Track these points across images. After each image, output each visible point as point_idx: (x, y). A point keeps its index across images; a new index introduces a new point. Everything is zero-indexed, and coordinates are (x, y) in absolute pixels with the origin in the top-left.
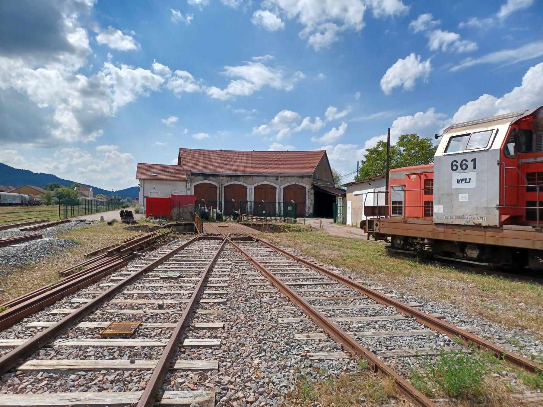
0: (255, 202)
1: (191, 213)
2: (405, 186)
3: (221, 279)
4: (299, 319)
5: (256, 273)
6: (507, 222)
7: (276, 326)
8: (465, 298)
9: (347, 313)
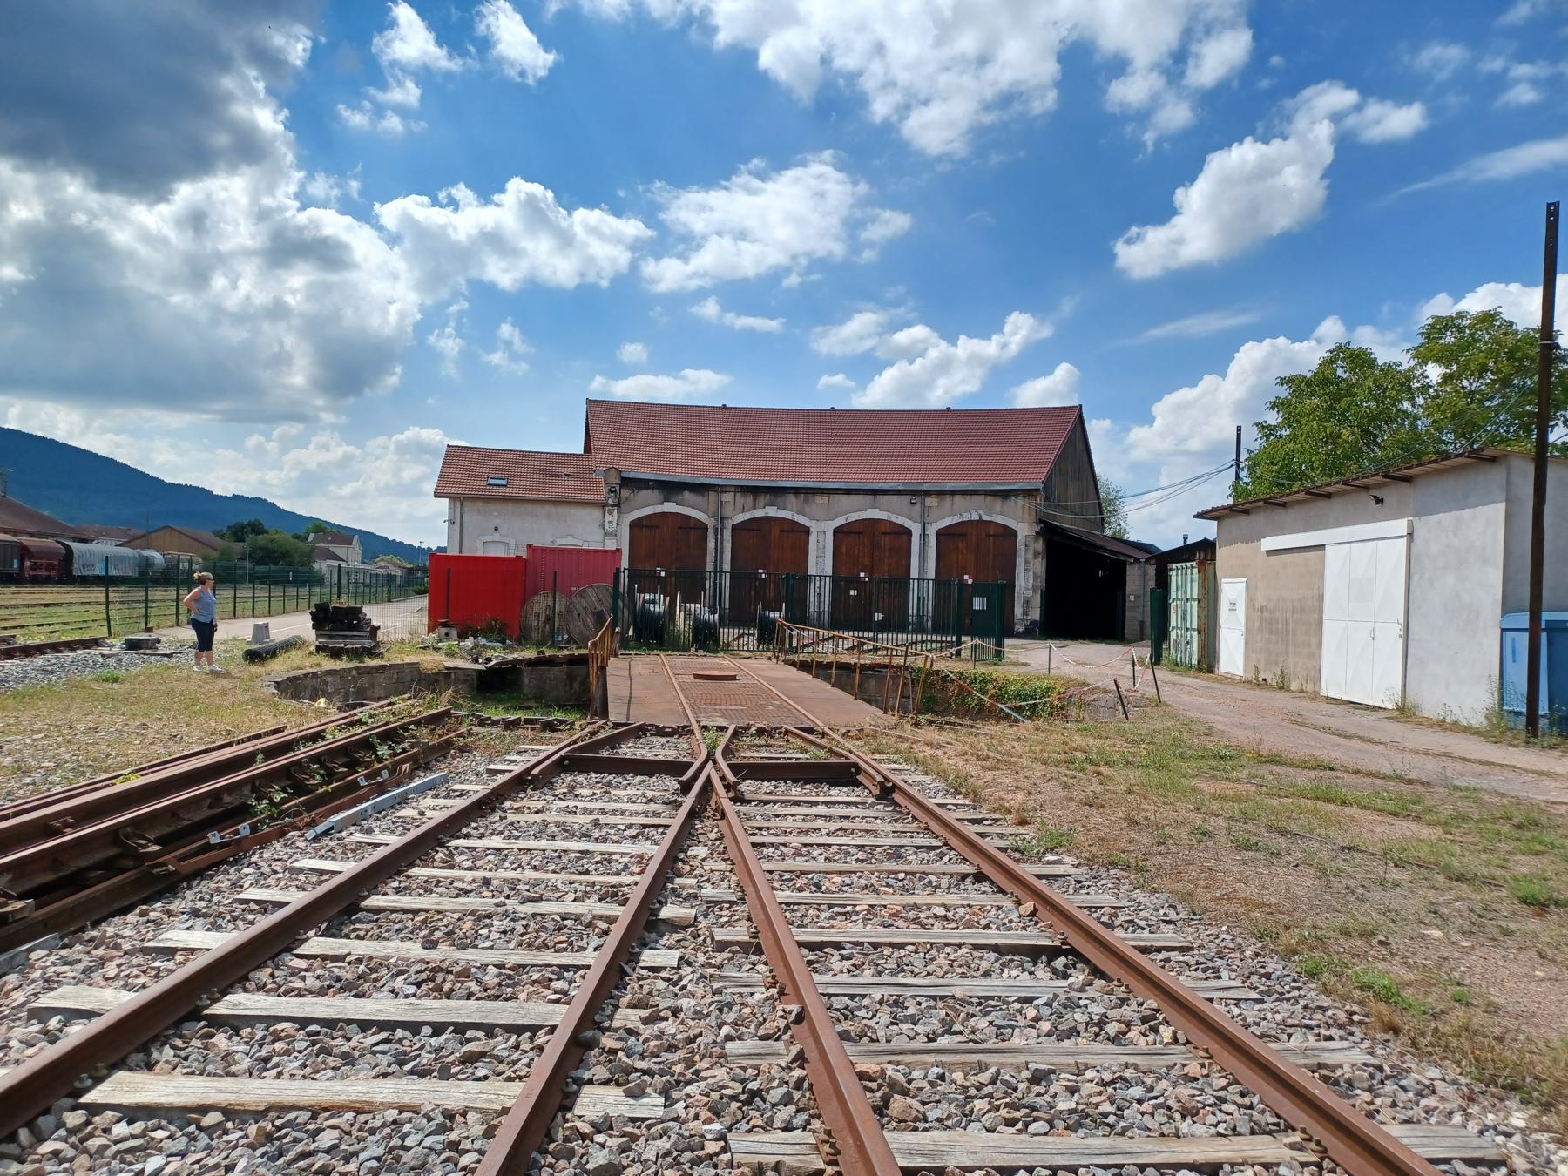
0: (835, 579)
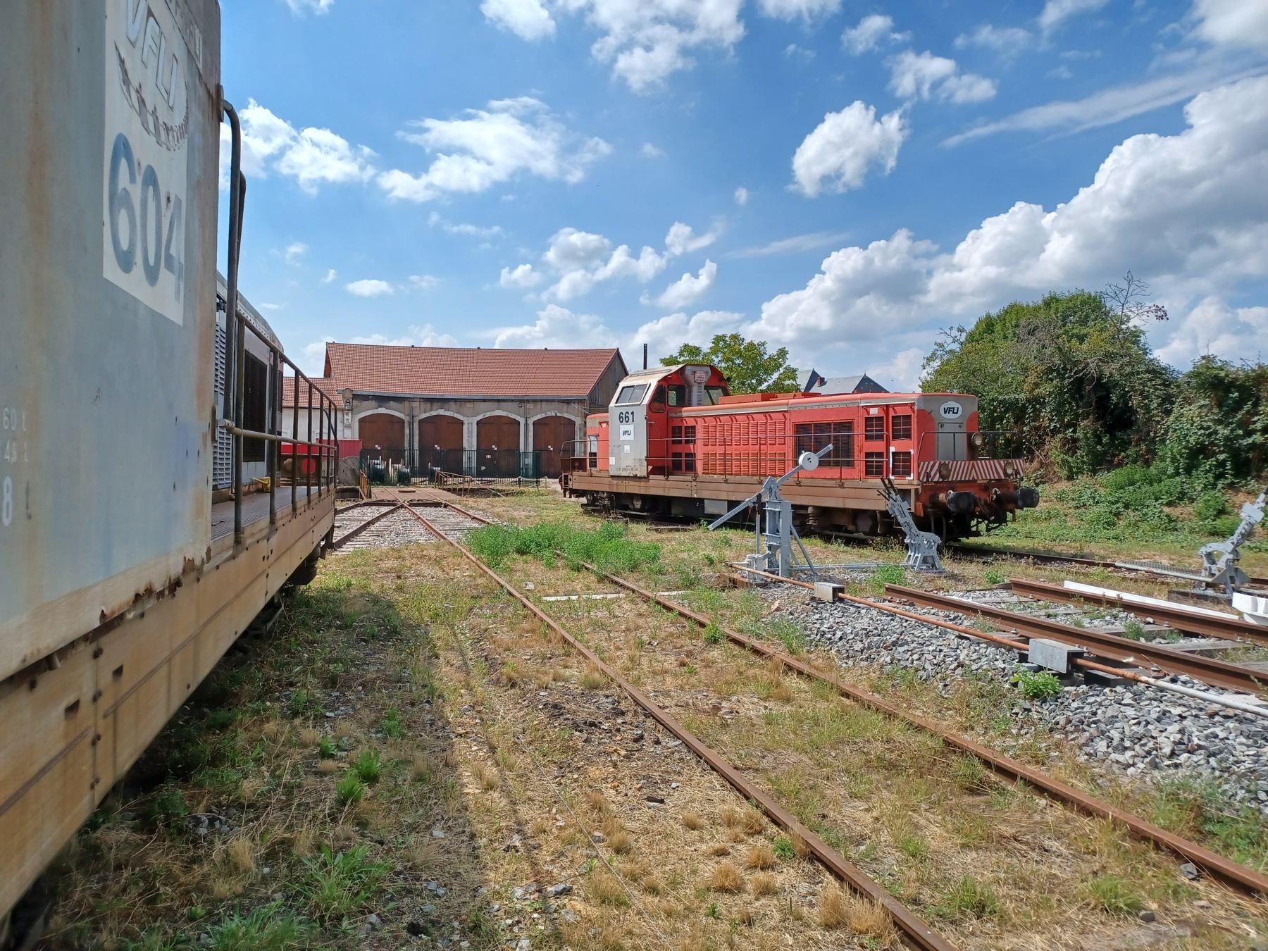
1: (353, 471)
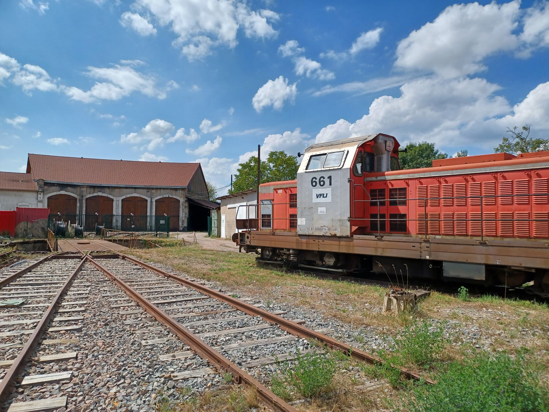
0: (122, 216)
1: (43, 229)
2: (273, 200)
3: (77, 302)
4: (165, 339)
5: (120, 293)
6: (356, 232)
7: (139, 349)
8: (323, 303)
9: (215, 328)
